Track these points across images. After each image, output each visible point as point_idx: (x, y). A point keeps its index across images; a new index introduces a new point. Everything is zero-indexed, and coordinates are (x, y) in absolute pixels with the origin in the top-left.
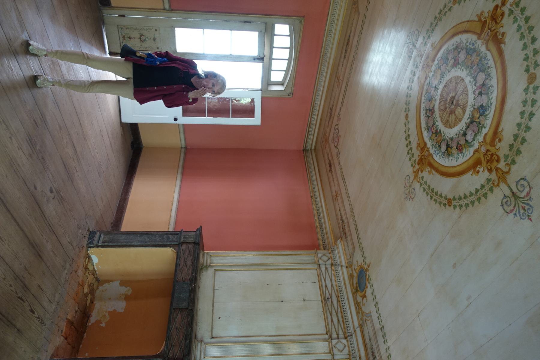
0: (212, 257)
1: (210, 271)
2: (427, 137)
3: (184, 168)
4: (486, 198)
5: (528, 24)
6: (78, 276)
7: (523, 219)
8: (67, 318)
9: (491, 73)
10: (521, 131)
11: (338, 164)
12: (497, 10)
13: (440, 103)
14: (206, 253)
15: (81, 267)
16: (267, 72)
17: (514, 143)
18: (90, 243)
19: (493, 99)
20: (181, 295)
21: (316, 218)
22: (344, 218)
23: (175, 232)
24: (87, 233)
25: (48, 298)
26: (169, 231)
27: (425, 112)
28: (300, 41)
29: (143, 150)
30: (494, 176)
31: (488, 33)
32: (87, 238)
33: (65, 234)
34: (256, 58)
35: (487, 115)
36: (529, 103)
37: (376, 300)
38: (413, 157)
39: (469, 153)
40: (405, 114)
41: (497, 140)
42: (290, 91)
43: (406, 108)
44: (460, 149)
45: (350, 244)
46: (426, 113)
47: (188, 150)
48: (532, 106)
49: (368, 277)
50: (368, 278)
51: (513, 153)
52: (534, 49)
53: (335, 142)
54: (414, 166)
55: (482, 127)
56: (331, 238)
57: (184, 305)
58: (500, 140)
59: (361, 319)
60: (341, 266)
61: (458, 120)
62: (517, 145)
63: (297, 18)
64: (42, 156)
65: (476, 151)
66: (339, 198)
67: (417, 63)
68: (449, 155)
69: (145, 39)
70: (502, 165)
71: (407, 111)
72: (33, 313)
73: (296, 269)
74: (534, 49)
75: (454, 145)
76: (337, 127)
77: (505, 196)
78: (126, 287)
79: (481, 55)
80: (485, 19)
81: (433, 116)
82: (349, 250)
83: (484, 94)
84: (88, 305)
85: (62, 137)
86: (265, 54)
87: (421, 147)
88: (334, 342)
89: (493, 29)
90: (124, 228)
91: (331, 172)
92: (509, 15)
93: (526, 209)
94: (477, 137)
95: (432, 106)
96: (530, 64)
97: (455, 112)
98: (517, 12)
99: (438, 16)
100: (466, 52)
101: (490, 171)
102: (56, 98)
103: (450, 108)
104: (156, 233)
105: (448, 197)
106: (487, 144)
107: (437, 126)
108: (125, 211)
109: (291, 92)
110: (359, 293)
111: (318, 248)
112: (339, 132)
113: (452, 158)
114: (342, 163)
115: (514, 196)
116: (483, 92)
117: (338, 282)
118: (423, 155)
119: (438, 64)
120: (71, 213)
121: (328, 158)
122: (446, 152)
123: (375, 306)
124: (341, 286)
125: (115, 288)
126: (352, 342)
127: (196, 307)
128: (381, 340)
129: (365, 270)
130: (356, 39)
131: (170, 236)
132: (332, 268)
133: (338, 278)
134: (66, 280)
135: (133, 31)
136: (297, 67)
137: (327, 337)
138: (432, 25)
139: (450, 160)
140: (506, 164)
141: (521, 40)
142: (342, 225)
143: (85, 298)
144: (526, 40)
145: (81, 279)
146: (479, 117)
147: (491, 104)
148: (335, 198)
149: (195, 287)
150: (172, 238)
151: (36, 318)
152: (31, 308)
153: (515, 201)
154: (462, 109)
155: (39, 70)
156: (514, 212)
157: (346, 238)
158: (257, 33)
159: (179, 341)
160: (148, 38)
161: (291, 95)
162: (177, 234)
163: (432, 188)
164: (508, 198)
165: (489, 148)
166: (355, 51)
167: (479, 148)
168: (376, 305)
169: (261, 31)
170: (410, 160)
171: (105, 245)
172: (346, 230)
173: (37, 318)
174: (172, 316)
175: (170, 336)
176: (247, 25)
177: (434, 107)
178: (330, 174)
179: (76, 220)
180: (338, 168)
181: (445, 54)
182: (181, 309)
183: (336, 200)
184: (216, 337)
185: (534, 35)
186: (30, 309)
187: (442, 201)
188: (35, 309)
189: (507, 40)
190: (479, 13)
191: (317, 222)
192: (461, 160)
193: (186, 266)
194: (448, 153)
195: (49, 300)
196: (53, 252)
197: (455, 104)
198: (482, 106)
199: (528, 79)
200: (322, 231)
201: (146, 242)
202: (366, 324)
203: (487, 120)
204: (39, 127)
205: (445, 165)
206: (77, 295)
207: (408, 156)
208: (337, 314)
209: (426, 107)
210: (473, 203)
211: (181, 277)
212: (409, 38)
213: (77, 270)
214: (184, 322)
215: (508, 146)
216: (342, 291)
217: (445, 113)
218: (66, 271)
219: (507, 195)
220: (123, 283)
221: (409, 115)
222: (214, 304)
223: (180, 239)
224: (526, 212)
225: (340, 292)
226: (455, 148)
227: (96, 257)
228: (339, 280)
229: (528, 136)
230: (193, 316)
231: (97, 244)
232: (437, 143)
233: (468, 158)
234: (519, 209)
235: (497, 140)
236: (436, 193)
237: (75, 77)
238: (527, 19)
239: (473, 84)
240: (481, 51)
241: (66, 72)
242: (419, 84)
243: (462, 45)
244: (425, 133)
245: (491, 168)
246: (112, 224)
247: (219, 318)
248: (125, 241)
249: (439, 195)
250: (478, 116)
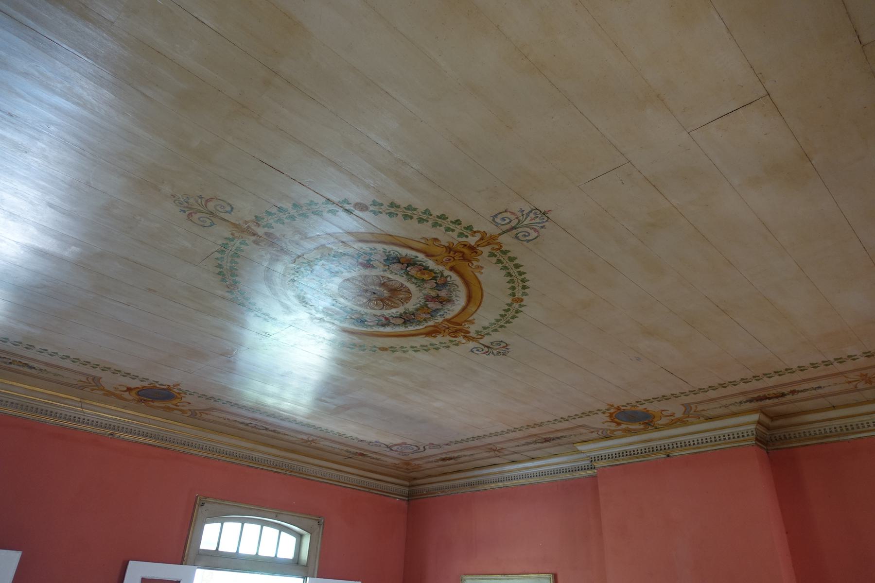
4: (515, 258)
11: (448, 446)
62: (446, 224)
91: (459, 457)
229: (436, 212)
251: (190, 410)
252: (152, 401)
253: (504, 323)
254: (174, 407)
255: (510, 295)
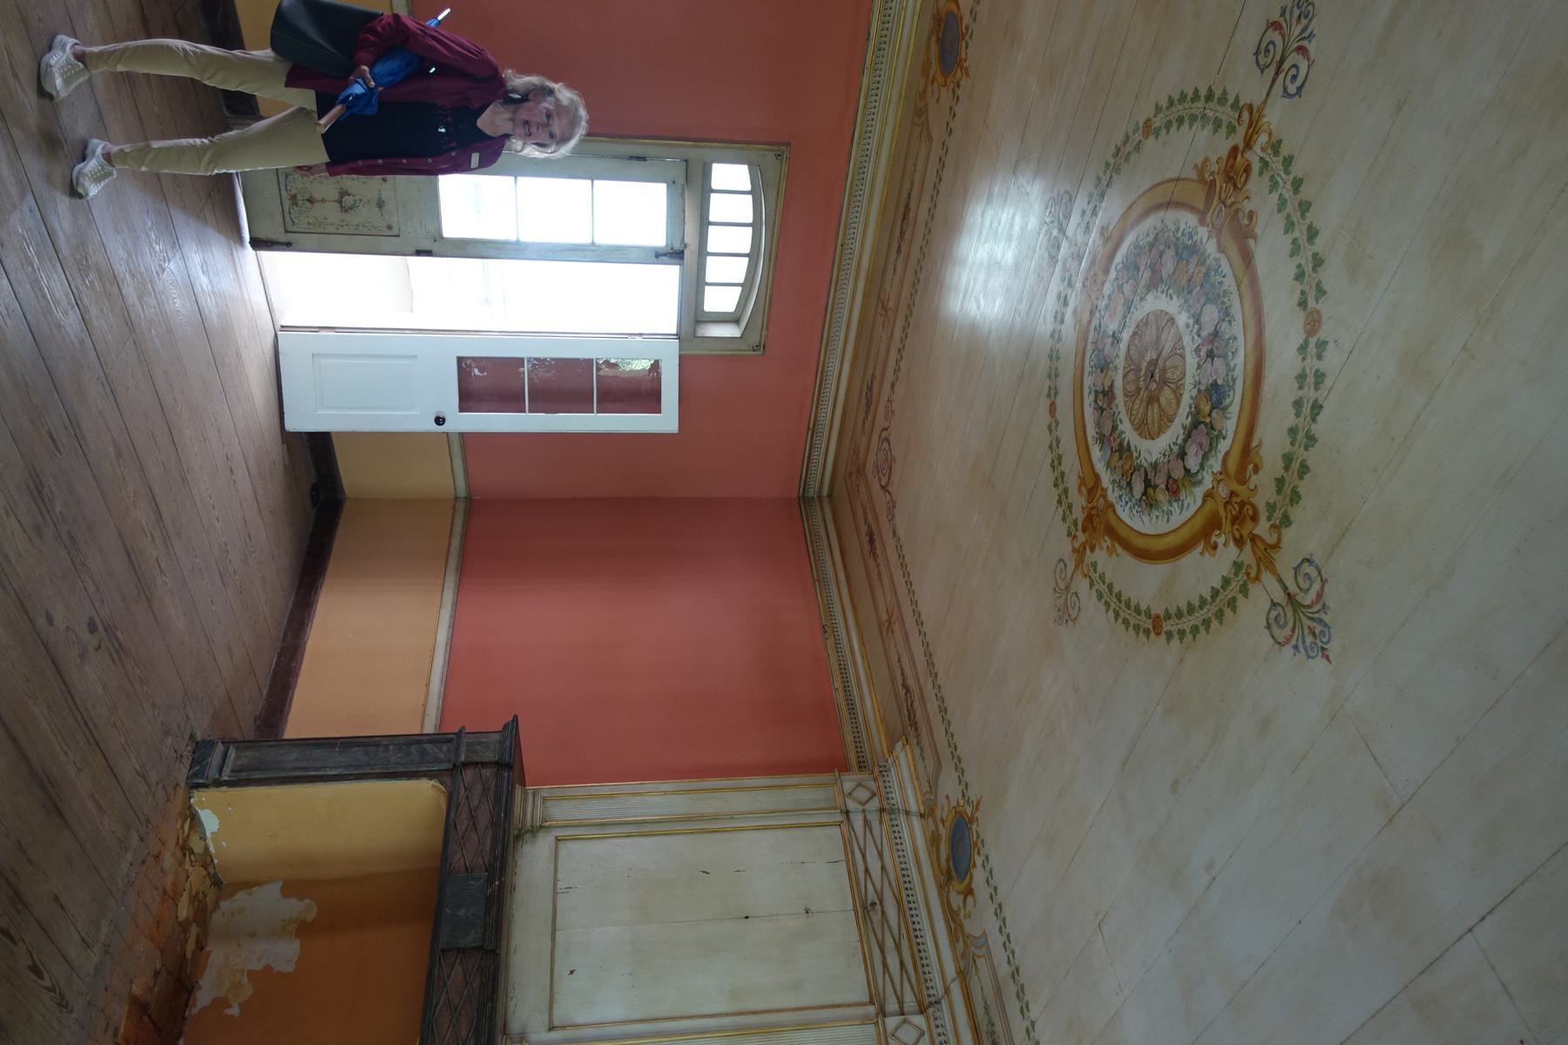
0: (548, 803)
1: (543, 844)
2: (1100, 461)
3: (463, 555)
4: (1234, 609)
5: (1298, 196)
6: (162, 870)
7: (1313, 658)
8: (129, 993)
9: (1231, 306)
10: (1297, 445)
11: (891, 535)
12: (1235, 158)
13: (1125, 376)
14: (530, 793)
15: (171, 843)
16: (694, 287)
17: (1285, 475)
18: (195, 775)
19: (1236, 371)
20: (462, 913)
21: (838, 684)
22: (911, 682)
23: (442, 737)
24: (187, 745)
25: (79, 932)
26: (426, 732)
27: (1092, 397)
28: (780, 208)
29: (346, 507)
30: (1247, 556)
31: (1221, 210)
32: (187, 762)
33: (128, 750)
34: (661, 252)
35: (1226, 408)
36: (1311, 379)
37: (999, 898)
38: (1071, 512)
39: (1193, 500)
40: (1048, 402)
41: (1251, 467)
42: (758, 340)
43: (1050, 387)
44: (1174, 490)
45: (928, 751)
46: (1096, 401)
47: (475, 506)
48: (1317, 389)
49: (975, 837)
50: (975, 839)
51: (1284, 499)
52: (1315, 255)
53: (881, 475)
54: (1075, 536)
55: (1217, 437)
56: (878, 738)
57: (471, 939)
58: (1256, 469)
59: (963, 956)
60: (907, 813)
61: (1167, 419)
63: (772, 147)
64: (69, 532)
65: (1208, 496)
66: (896, 627)
67: (1071, 275)
68: (1151, 506)
69: (353, 203)
70: (1262, 528)
71: (1053, 393)
72: (39, 974)
73: (783, 827)
74: (1315, 255)
75: (1160, 481)
76: (884, 435)
77: (1274, 604)
78: (301, 899)
79: (1208, 262)
80: (1211, 178)
81: (1111, 409)
82: (925, 767)
83: (1218, 357)
84: (189, 955)
85: (124, 478)
86: (687, 241)
87: (1090, 486)
88: (892, 1022)
89: (1229, 202)
90: (295, 727)
92: (1261, 173)
93: (1317, 634)
94: (1208, 459)
95: (1107, 384)
96: (1306, 288)
97: (1158, 400)
98: (1277, 164)
99: (1112, 161)
100: (1177, 253)
101: (1239, 542)
102: (107, 372)
103: (1147, 388)
104: (388, 739)
105: (1153, 613)
106: (1230, 478)
107: (1122, 432)
108: (296, 683)
109: (760, 342)
110: (955, 883)
111: (844, 768)
112: (890, 449)
113: (1158, 514)
114: (901, 532)
115: (1292, 603)
116: (1215, 351)
117: (900, 857)
118: (1093, 507)
119: (1117, 279)
120: (145, 688)
121: (866, 519)
122: (1144, 498)
123: (996, 915)
124: (907, 869)
125: (269, 902)
126: (938, 1022)
127: (504, 943)
128: (1013, 1006)
129: (967, 820)
130: (926, 204)
131: (427, 746)
132: (881, 822)
133: (900, 847)
134: (129, 882)
135: (321, 183)
136: (774, 274)
137: (872, 1009)
138: (1099, 183)
139: (1155, 517)
140: (1272, 526)
141: (1286, 232)
142: (907, 700)
143: (182, 936)
144: (1296, 234)
145: (169, 879)
146: (1211, 411)
147: (1234, 380)
148: (887, 627)
149: (502, 887)
150: (435, 753)
151: (45, 991)
152: (33, 961)
153: (1294, 615)
154: (1174, 391)
155: (64, 298)
156: (1293, 642)
157: (918, 736)
158: (665, 185)
159: (458, 1040)
160: (361, 200)
161: (760, 349)
162: (450, 741)
163: (1116, 589)
164: (1279, 608)
165: (1235, 486)
166: (924, 235)
167: (1213, 488)
168: (998, 911)
169: (674, 182)
170: (1064, 519)
171: (239, 780)
172: (918, 712)
173: (49, 990)
174: (436, 972)
175: (432, 1029)
176: (634, 165)
177: (1112, 386)
178: (871, 561)
179: (157, 710)
180: (890, 543)
181: (1132, 256)
182: (462, 951)
183: (890, 633)
184: (564, 1027)
185: (1312, 223)
186: (30, 962)
187: (1141, 623)
188: (42, 964)
189: (1258, 230)
190: (1199, 160)
191: (840, 698)
192: (1178, 519)
193: (476, 828)
194: (1148, 501)
195: (83, 940)
196: (96, 801)
197: (1157, 379)
198: (1215, 385)
199: (1307, 323)
200: (853, 721)
201: (358, 767)
202: (976, 967)
203: (1227, 418)
204: (62, 450)
205: (1143, 532)
206: (158, 926)
207: (1061, 510)
208: (898, 947)
209: (1094, 386)
210: (1207, 623)
211: (462, 861)
212: (1050, 212)
213: (160, 853)
214: (472, 987)
215: (1273, 480)
216: (910, 882)
217: (1138, 401)
218: (129, 856)
219: (1278, 601)
220: (291, 889)
221: (1058, 403)
222: (557, 934)
223: (457, 753)
224: (1318, 641)
225: (906, 886)
226: (1161, 488)
227: (214, 816)
228: (901, 853)
229: (1313, 457)
230: (497, 968)
231: (217, 776)
232: (1123, 476)
233: (1192, 513)
234: (1303, 634)
235: (1251, 467)
236: (1125, 604)
237: (158, 310)
238: (1297, 184)
239: (1194, 331)
240: (1207, 253)
241: (136, 299)
242: (1077, 328)
243: (1166, 235)
244: (1096, 452)
245: (1241, 536)
246: (258, 722)
247: (572, 972)
248: (300, 764)
249: (1133, 608)
250: (1208, 408)
251: (926, 105)
252: (938, 39)
253: (1114, 609)
254: (931, 77)
255: (1167, 611)
